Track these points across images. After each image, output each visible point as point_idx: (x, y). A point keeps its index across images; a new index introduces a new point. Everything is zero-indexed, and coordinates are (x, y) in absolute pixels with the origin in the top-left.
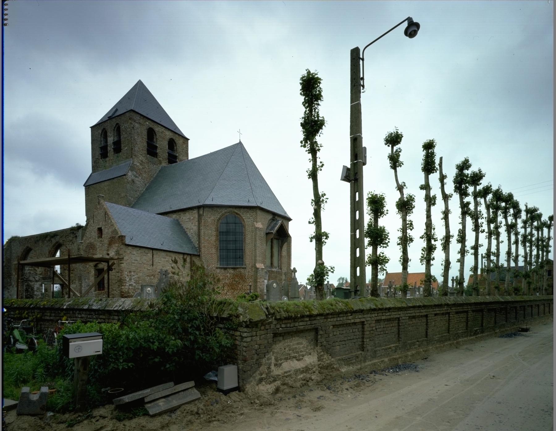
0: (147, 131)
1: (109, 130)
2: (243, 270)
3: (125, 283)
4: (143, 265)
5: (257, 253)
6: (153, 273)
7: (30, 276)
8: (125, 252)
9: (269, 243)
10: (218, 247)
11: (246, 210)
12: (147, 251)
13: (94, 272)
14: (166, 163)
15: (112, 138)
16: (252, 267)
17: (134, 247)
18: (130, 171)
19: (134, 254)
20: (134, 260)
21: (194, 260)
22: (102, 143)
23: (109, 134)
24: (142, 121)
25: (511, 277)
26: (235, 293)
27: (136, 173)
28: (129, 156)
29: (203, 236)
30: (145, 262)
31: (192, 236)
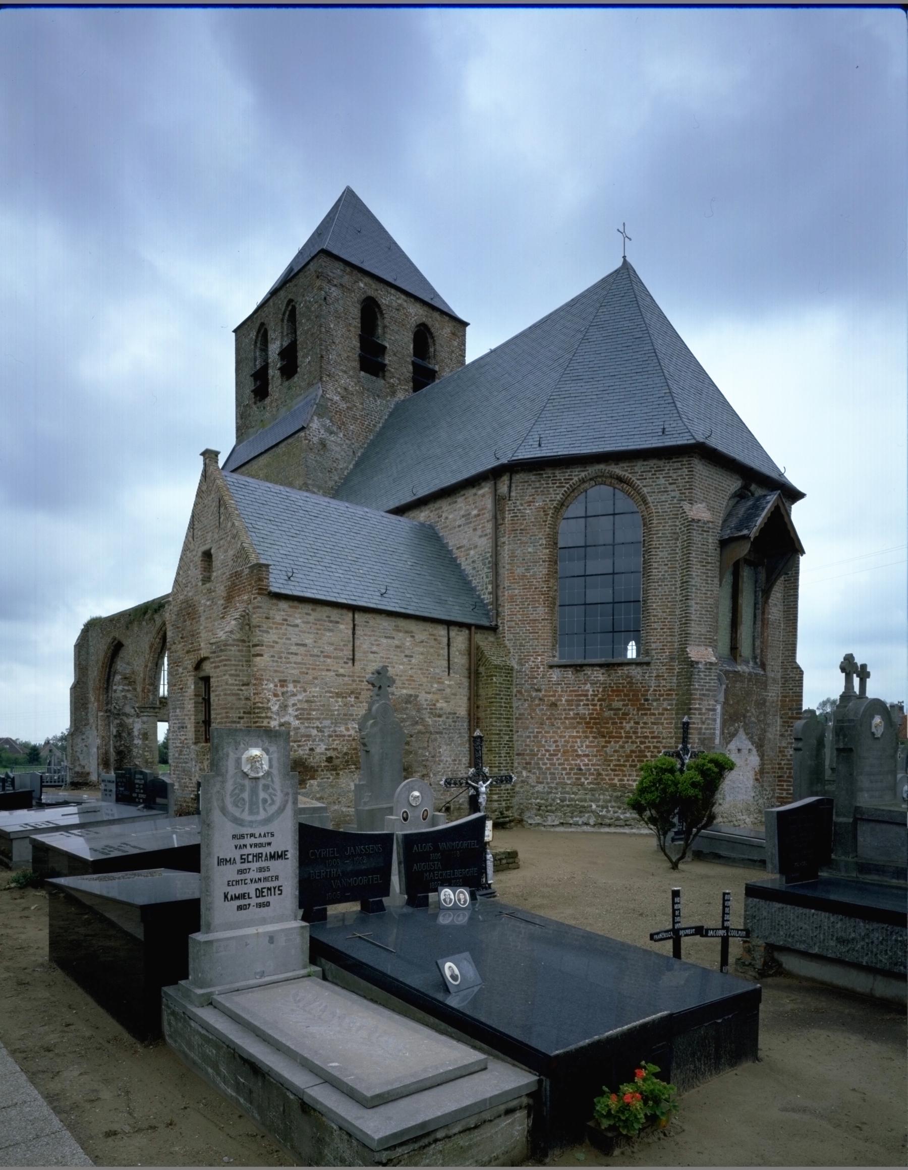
0: (359, 306)
1: (272, 324)
2: (639, 669)
3: (267, 717)
4: (322, 659)
5: (692, 610)
6: (354, 686)
7: (125, 704)
8: (267, 618)
9: (728, 579)
10: (554, 599)
11: (652, 463)
12: (335, 614)
13: (193, 687)
14: (406, 390)
15: (278, 343)
16: (672, 659)
17: (296, 604)
18: (315, 418)
19: (297, 626)
20: (297, 644)
21: (481, 643)
22: (257, 363)
23: (271, 335)
24: (347, 280)
25: (186, 727)
26: (608, 750)
27: (331, 421)
28: (315, 378)
29: (507, 567)
30: (329, 649)
31: (474, 568)
